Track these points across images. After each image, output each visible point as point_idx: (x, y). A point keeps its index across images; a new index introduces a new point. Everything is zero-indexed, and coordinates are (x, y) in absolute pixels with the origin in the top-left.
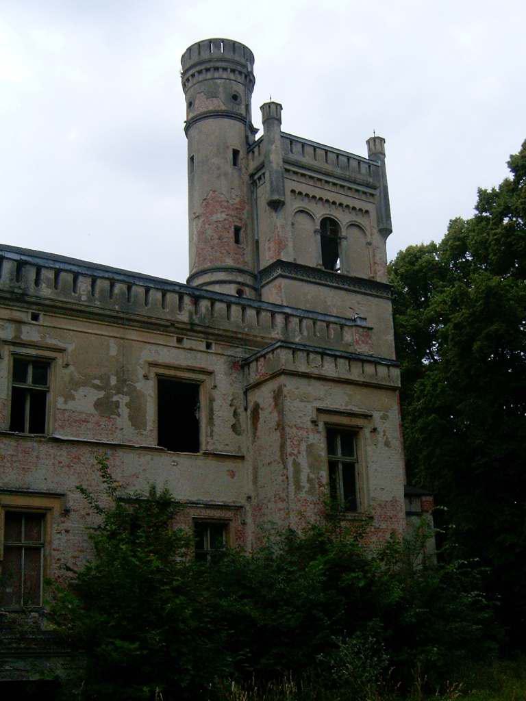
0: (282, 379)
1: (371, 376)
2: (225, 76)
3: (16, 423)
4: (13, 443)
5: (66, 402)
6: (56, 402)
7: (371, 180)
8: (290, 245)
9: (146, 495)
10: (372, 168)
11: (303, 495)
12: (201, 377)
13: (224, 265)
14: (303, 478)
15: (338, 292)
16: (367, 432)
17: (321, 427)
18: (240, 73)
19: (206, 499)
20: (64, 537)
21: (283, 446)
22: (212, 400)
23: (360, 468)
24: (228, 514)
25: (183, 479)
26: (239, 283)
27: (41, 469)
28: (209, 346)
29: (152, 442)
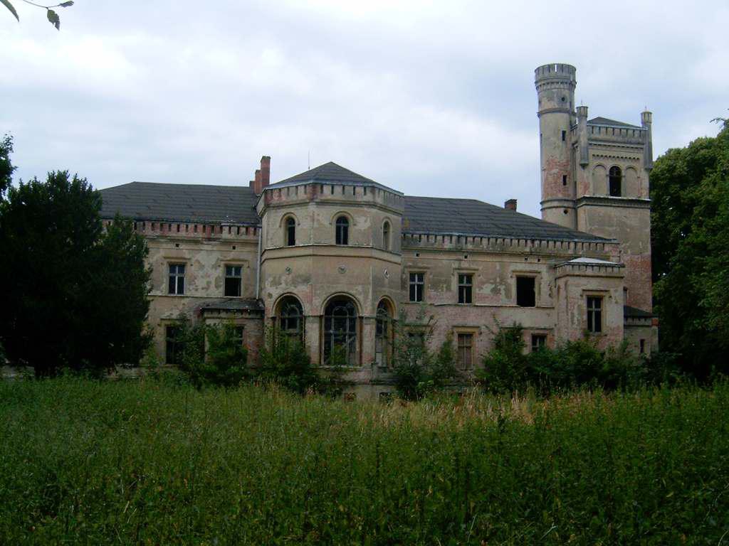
0: (568, 278)
1: (610, 273)
2: (557, 87)
3: (461, 300)
4: (460, 309)
5: (479, 290)
6: (476, 291)
7: (640, 140)
8: (591, 186)
9: (512, 326)
10: (642, 132)
11: (575, 326)
12: (536, 274)
13: (558, 198)
14: (575, 319)
15: (619, 209)
16: (606, 298)
17: (584, 297)
18: (566, 83)
19: (537, 326)
20: (480, 343)
21: (567, 306)
22: (540, 284)
23: (603, 314)
24: (546, 332)
25: (527, 318)
26: (565, 207)
27: (471, 317)
28: (539, 260)
29: (513, 301)
